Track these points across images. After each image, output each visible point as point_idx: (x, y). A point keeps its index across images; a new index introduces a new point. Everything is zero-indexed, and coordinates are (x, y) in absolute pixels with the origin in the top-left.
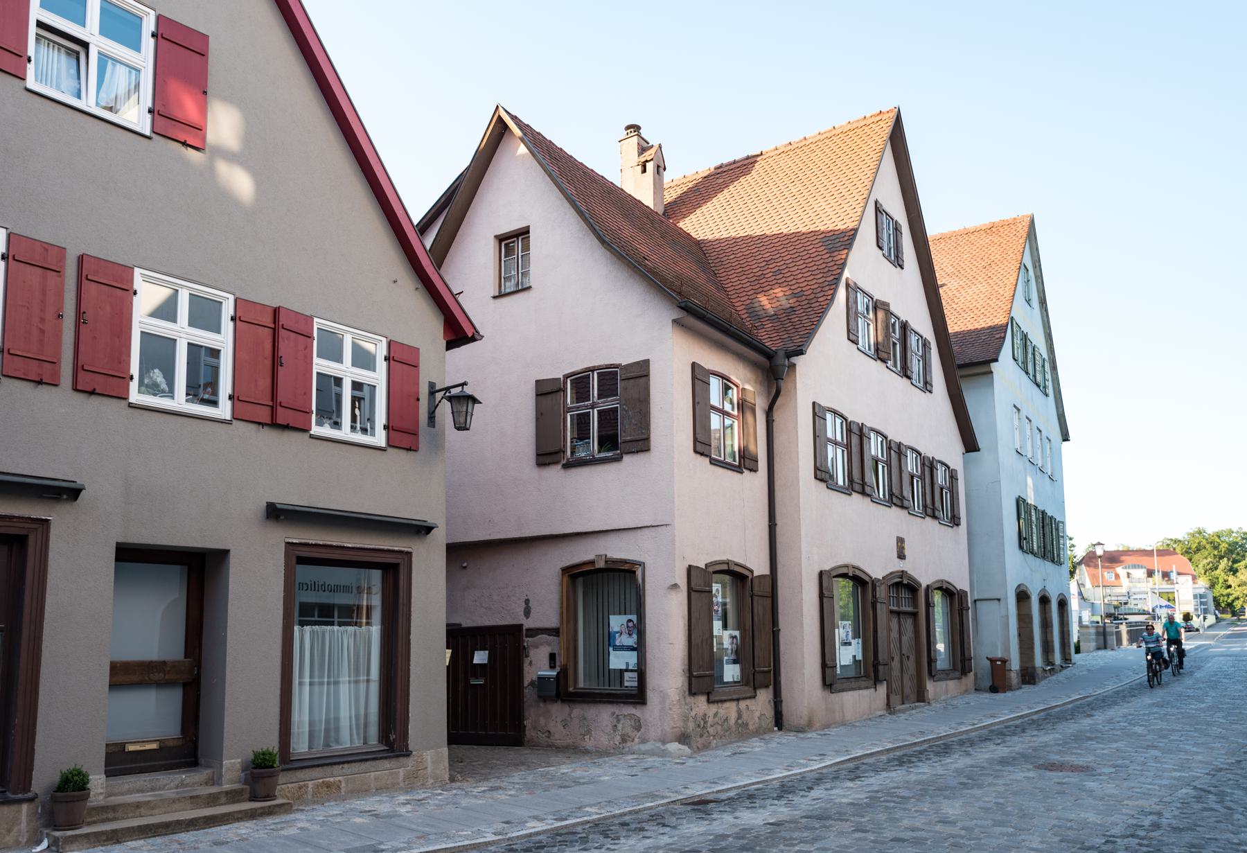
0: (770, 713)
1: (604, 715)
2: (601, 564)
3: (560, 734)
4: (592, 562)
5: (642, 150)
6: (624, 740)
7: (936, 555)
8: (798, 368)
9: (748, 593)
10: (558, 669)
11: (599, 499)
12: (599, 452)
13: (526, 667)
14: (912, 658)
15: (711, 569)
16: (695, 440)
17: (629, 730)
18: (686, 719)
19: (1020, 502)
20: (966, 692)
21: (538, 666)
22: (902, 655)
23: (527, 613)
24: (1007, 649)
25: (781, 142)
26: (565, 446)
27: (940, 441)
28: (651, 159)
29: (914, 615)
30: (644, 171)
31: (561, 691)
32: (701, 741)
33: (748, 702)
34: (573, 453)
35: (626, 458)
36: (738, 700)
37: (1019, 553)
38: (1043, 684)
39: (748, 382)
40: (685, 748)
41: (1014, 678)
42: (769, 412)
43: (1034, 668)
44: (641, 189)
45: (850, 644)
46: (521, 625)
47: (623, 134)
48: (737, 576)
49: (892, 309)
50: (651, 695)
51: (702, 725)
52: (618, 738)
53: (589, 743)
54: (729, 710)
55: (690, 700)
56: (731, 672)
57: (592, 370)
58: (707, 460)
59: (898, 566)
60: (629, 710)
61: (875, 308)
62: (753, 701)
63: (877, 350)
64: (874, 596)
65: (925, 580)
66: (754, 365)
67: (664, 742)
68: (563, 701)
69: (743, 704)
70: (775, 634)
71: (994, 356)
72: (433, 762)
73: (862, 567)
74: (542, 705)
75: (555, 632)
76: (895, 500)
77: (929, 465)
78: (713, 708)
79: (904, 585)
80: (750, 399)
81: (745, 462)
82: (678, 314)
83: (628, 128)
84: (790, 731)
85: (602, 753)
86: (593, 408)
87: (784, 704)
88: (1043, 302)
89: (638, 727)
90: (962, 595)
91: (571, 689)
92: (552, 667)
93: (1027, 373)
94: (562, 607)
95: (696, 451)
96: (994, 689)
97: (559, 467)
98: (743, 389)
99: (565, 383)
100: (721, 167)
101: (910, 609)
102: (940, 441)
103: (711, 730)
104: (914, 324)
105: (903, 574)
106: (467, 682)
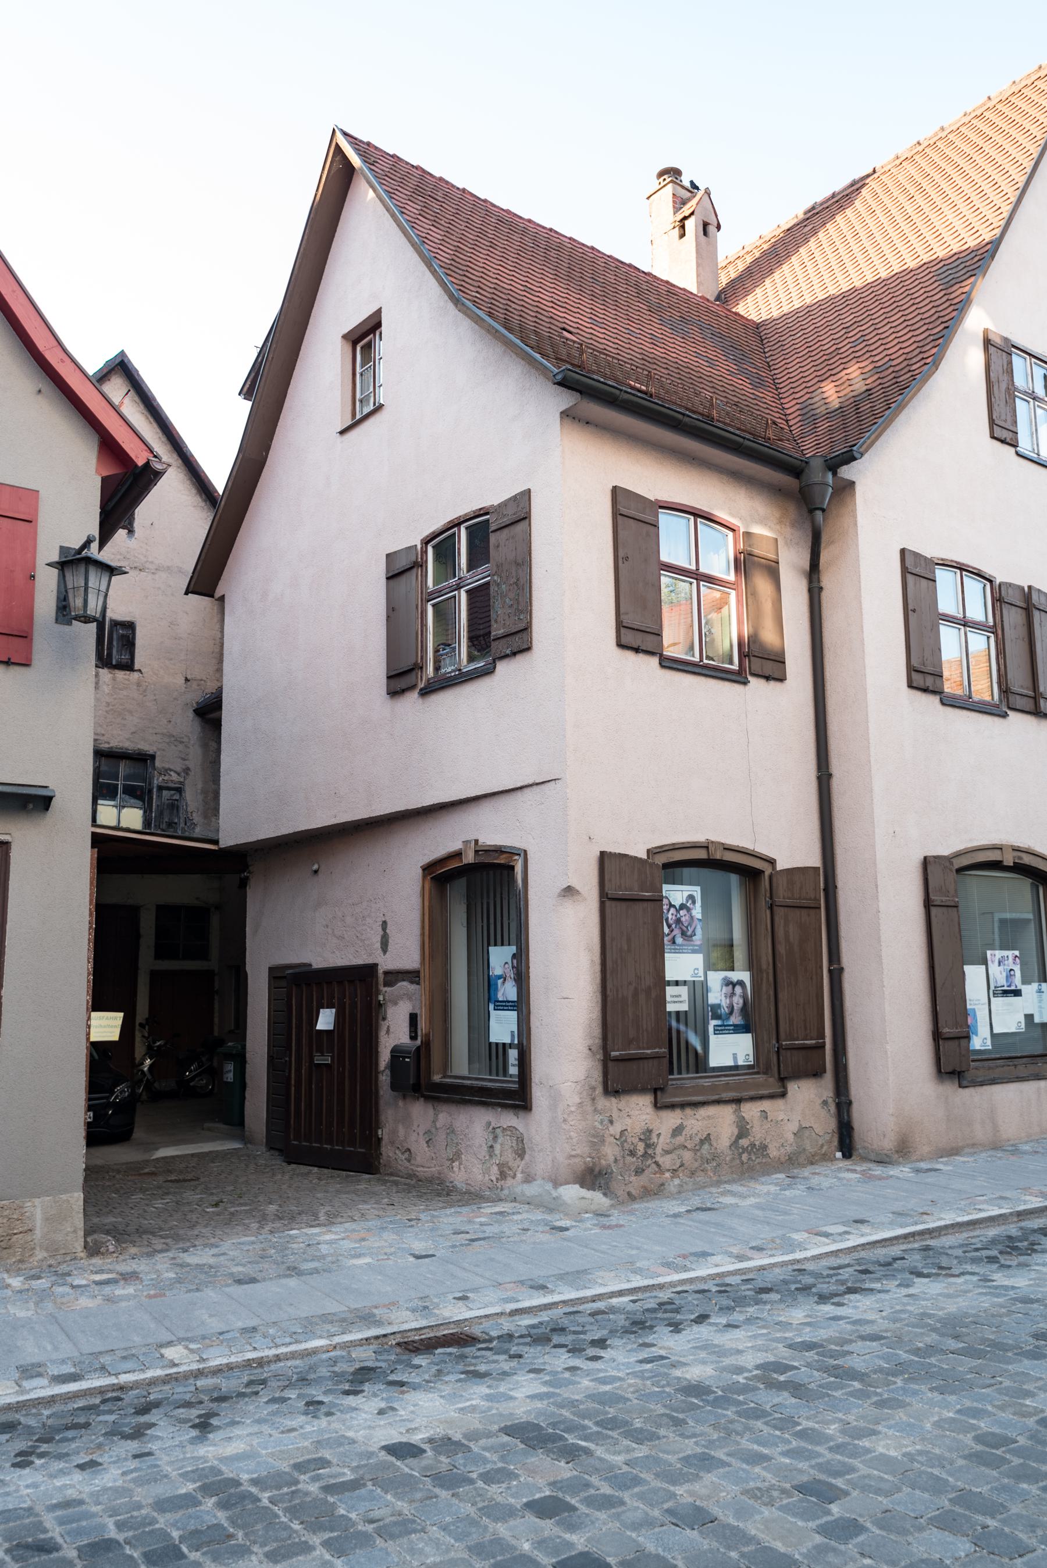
0: (825, 1124)
1: (475, 1124)
2: (469, 858)
3: (425, 1158)
4: (458, 855)
5: (679, 203)
6: (503, 1176)
8: (859, 489)
10: (418, 1042)
11: (466, 744)
12: (471, 659)
13: (382, 1033)
15: (661, 860)
16: (620, 625)
17: (509, 1156)
18: (597, 1140)
21: (395, 1032)
23: (385, 946)
25: (903, 146)
26: (424, 657)
30: (682, 235)
31: (421, 1077)
32: (636, 1183)
33: (766, 1105)
34: (437, 669)
35: (502, 667)
36: (738, 1101)
39: (762, 521)
40: (597, 1198)
42: (813, 571)
44: (675, 264)
45: (1017, 993)
46: (376, 965)
47: (655, 184)
48: (738, 871)
50: (539, 1095)
51: (643, 1151)
52: (495, 1170)
53: (458, 1177)
54: (719, 1122)
55: (603, 1102)
56: (729, 1049)
57: (456, 524)
58: (654, 661)
60: (508, 1119)
62: (780, 1103)
66: (777, 492)
67: (556, 1184)
68: (427, 1098)
69: (751, 1111)
70: (837, 975)
72: (47, 1219)
74: (401, 1103)
75: (412, 976)
78: (671, 1119)
80: (763, 550)
81: (758, 662)
82: (566, 400)
83: (661, 174)
84: (865, 1159)
85: (472, 1197)
86: (458, 588)
89: (521, 1153)
91: (437, 1078)
92: (413, 1038)
94: (423, 934)
95: (910, 686)
97: (414, 695)
98: (747, 535)
99: (425, 552)
100: (813, 208)
103: (666, 1161)
106: (311, 1058)
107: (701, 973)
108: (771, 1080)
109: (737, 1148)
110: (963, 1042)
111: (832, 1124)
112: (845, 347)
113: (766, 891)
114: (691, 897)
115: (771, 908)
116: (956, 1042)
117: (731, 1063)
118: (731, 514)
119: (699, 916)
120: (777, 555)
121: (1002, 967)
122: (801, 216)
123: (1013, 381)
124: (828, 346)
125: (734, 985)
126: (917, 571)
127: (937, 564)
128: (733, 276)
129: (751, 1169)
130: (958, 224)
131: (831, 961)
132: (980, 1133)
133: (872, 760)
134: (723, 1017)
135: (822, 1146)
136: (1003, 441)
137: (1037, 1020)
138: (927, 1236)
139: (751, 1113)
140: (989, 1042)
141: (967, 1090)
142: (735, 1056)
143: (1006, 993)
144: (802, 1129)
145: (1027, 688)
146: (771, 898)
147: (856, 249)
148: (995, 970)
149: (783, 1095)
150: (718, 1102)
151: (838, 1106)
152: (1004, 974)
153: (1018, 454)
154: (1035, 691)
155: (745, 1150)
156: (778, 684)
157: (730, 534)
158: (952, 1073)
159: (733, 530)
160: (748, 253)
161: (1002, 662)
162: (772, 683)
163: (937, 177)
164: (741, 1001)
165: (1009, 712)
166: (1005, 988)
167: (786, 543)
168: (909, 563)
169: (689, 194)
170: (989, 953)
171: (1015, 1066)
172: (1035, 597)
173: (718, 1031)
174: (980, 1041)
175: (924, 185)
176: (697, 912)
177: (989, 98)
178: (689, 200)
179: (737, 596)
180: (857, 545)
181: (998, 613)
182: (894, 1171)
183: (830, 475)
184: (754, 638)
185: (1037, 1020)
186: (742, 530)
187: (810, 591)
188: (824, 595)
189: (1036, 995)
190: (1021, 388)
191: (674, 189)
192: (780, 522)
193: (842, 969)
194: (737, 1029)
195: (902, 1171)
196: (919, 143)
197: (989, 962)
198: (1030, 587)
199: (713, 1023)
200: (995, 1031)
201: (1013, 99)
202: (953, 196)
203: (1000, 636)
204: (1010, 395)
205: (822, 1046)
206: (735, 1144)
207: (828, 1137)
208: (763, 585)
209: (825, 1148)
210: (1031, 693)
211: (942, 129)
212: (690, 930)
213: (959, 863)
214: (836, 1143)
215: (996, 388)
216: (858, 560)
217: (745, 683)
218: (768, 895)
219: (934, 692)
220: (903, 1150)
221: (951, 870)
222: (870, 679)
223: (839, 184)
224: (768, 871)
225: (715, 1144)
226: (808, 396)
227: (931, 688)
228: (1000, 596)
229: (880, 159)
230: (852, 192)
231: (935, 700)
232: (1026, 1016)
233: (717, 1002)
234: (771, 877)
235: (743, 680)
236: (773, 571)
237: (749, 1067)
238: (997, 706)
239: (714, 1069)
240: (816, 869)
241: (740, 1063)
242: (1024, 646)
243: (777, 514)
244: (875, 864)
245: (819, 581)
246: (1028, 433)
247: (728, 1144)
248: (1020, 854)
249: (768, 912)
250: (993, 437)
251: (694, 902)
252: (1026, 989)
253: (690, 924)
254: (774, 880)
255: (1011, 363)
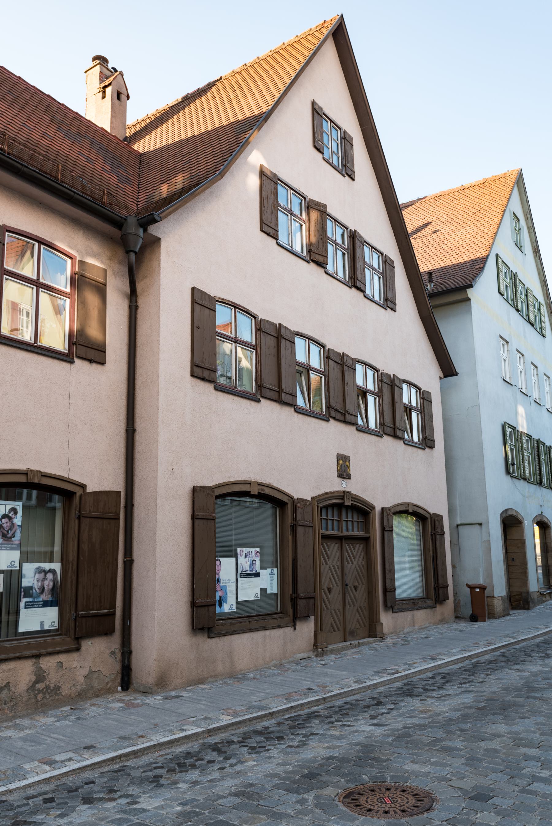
0: (110, 668)
5: (103, 77)
7: (389, 475)
9: (74, 514)
14: (362, 589)
19: (509, 432)
20: (443, 621)
22: (345, 586)
24: (489, 574)
27: (415, 365)
28: (113, 83)
29: (366, 540)
30: (104, 97)
33: (62, 658)
36: (38, 656)
37: (507, 479)
38: (539, 608)
39: (95, 256)
41: (498, 605)
42: (133, 295)
43: (528, 593)
44: (98, 113)
45: (257, 575)
49: (329, 210)
58: (293, 409)
59: (338, 485)
61: (308, 208)
63: (309, 251)
64: (294, 519)
65: (380, 499)
71: (469, 283)
73: (276, 485)
76: (333, 413)
77: (390, 385)
79: (347, 509)
81: (84, 348)
83: (95, 58)
84: (137, 691)
87: (134, 655)
88: (536, 251)
90: (437, 519)
93: (518, 310)
95: (192, 375)
96: (474, 618)
98: (81, 263)
101: (361, 534)
102: (415, 365)
104: (365, 233)
105: (344, 494)
107: (17, 564)
108: (68, 639)
109: (33, 691)
110: (211, 608)
111: (117, 667)
112: (179, 165)
113: (76, 506)
114: (14, 510)
115: (79, 518)
116: (206, 608)
117: (38, 628)
118: (70, 247)
119: (20, 523)
120: (106, 280)
121: (247, 559)
122: (180, 100)
123: (277, 200)
124: (171, 165)
125: (46, 572)
126: (202, 302)
127: (218, 301)
128: (138, 129)
129: (44, 705)
130: (253, 104)
131: (125, 555)
132: (220, 668)
133: (160, 420)
134: (34, 595)
135: (108, 683)
136: (268, 234)
137: (269, 592)
138: (133, 756)
139: (49, 664)
140: (234, 607)
141: (214, 640)
142: (42, 624)
143: (249, 575)
144: (91, 672)
145: (274, 386)
146: (80, 511)
147: (201, 116)
148: (242, 560)
149: (78, 649)
150: (20, 658)
151: (123, 654)
152: (249, 563)
153: (278, 244)
154: (279, 388)
155: (40, 691)
156: (99, 367)
157: (69, 261)
158: (202, 629)
159: (71, 258)
160: (149, 118)
161: (259, 368)
162: (94, 365)
163: (249, 81)
164: (51, 584)
165: (261, 399)
166: (249, 572)
167: (114, 274)
168: (196, 297)
169: (111, 73)
170: (239, 550)
171: (250, 622)
172: (283, 331)
173: (28, 606)
174: (229, 606)
175: (242, 85)
176: (18, 520)
177: (284, 43)
178: (110, 76)
179: (71, 303)
180: (160, 280)
181: (258, 337)
182: (149, 700)
183: (141, 231)
184: (81, 332)
185: (269, 592)
186: (78, 259)
187: (130, 307)
188: (139, 311)
189: (269, 576)
190: (283, 206)
191: (101, 68)
192: (110, 259)
193: (133, 560)
194: (46, 604)
195: (155, 700)
196: (245, 65)
197: (239, 556)
198: (280, 324)
199: (24, 600)
200: (239, 600)
201: (295, 44)
202: (254, 90)
203: (259, 352)
204: (274, 206)
205: (114, 614)
206: (32, 687)
207: (113, 677)
208: (92, 299)
209: (110, 684)
210: (277, 389)
211: (258, 58)
212: (10, 533)
213: (218, 492)
214: (119, 680)
215: (265, 201)
216: (159, 289)
217: (72, 362)
218: (78, 509)
219: (210, 381)
220: (162, 683)
221: (212, 496)
222: (162, 367)
223: (201, 84)
224: (79, 492)
225: (13, 690)
226: (153, 191)
227: (207, 378)
228: (261, 327)
229: (225, 72)
230: (208, 89)
231: (210, 387)
232: (261, 589)
233: (30, 585)
234: (81, 497)
235: (69, 360)
236: (101, 290)
237: (57, 630)
238: (254, 395)
239: (24, 633)
240: (119, 493)
241: (46, 628)
242: (274, 360)
243: (108, 254)
244: (156, 490)
245: (136, 302)
246: (286, 234)
247: (25, 688)
248: (262, 487)
249: (77, 521)
250: (262, 231)
251: (16, 513)
252: (263, 573)
253: (10, 529)
254: (83, 499)
255: (277, 189)
